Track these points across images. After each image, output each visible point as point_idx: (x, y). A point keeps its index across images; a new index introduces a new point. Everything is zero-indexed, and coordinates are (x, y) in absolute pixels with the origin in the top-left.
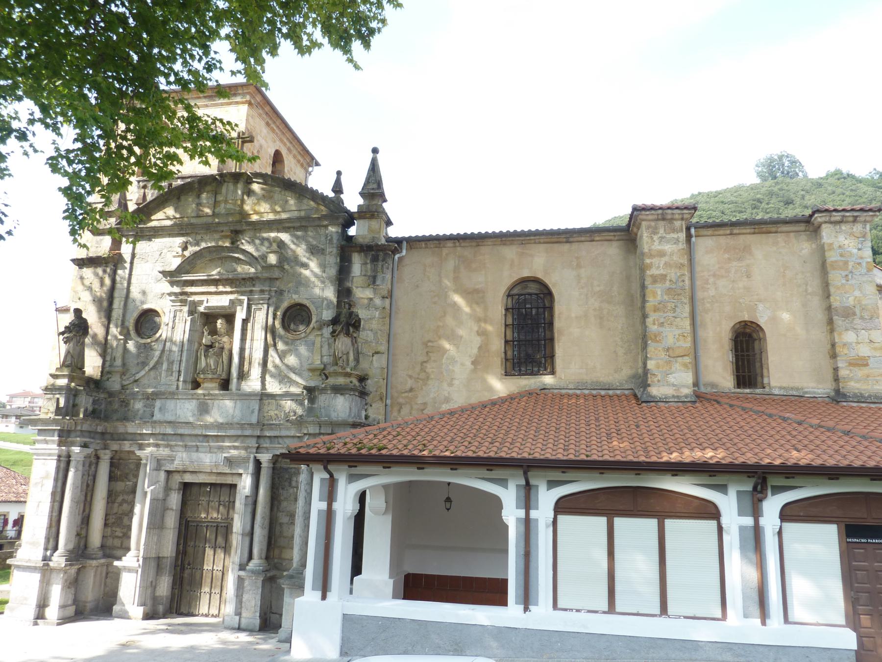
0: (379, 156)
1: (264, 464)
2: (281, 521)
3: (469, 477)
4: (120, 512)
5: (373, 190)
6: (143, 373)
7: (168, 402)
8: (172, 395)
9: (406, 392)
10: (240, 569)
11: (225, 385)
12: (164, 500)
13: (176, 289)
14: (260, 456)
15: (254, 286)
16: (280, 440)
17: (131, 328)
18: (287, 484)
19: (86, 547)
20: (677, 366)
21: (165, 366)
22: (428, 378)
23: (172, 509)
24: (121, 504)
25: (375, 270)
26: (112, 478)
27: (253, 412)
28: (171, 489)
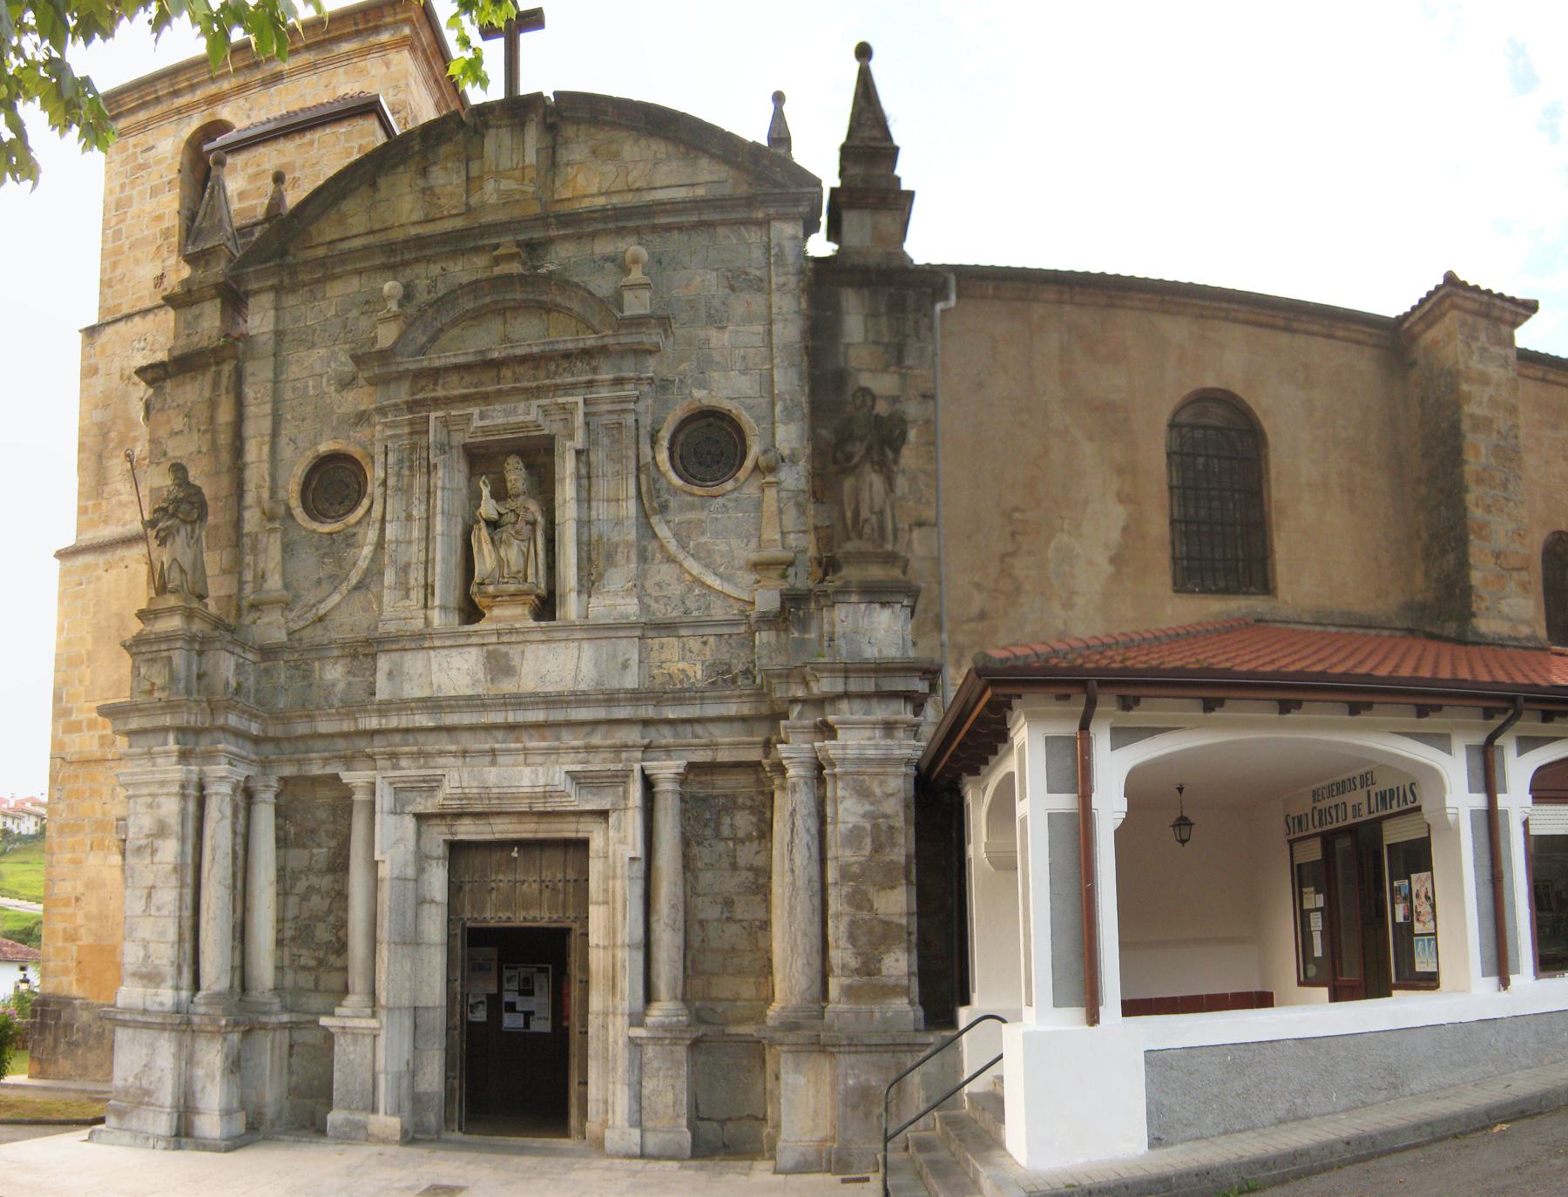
0: (874, 65)
1: (666, 787)
2: (701, 916)
3: (1375, 728)
4: (306, 914)
5: (869, 143)
6: (336, 598)
7: (408, 656)
8: (420, 640)
9: (971, 620)
10: (631, 1025)
11: (546, 607)
13: (402, 393)
14: (653, 767)
16: (699, 729)
17: (295, 503)
18: (708, 832)
19: (244, 988)
20: (1512, 586)
21: (389, 577)
22: (1018, 590)
24: (305, 897)
26: (282, 842)
27: (625, 666)
28: (428, 857)
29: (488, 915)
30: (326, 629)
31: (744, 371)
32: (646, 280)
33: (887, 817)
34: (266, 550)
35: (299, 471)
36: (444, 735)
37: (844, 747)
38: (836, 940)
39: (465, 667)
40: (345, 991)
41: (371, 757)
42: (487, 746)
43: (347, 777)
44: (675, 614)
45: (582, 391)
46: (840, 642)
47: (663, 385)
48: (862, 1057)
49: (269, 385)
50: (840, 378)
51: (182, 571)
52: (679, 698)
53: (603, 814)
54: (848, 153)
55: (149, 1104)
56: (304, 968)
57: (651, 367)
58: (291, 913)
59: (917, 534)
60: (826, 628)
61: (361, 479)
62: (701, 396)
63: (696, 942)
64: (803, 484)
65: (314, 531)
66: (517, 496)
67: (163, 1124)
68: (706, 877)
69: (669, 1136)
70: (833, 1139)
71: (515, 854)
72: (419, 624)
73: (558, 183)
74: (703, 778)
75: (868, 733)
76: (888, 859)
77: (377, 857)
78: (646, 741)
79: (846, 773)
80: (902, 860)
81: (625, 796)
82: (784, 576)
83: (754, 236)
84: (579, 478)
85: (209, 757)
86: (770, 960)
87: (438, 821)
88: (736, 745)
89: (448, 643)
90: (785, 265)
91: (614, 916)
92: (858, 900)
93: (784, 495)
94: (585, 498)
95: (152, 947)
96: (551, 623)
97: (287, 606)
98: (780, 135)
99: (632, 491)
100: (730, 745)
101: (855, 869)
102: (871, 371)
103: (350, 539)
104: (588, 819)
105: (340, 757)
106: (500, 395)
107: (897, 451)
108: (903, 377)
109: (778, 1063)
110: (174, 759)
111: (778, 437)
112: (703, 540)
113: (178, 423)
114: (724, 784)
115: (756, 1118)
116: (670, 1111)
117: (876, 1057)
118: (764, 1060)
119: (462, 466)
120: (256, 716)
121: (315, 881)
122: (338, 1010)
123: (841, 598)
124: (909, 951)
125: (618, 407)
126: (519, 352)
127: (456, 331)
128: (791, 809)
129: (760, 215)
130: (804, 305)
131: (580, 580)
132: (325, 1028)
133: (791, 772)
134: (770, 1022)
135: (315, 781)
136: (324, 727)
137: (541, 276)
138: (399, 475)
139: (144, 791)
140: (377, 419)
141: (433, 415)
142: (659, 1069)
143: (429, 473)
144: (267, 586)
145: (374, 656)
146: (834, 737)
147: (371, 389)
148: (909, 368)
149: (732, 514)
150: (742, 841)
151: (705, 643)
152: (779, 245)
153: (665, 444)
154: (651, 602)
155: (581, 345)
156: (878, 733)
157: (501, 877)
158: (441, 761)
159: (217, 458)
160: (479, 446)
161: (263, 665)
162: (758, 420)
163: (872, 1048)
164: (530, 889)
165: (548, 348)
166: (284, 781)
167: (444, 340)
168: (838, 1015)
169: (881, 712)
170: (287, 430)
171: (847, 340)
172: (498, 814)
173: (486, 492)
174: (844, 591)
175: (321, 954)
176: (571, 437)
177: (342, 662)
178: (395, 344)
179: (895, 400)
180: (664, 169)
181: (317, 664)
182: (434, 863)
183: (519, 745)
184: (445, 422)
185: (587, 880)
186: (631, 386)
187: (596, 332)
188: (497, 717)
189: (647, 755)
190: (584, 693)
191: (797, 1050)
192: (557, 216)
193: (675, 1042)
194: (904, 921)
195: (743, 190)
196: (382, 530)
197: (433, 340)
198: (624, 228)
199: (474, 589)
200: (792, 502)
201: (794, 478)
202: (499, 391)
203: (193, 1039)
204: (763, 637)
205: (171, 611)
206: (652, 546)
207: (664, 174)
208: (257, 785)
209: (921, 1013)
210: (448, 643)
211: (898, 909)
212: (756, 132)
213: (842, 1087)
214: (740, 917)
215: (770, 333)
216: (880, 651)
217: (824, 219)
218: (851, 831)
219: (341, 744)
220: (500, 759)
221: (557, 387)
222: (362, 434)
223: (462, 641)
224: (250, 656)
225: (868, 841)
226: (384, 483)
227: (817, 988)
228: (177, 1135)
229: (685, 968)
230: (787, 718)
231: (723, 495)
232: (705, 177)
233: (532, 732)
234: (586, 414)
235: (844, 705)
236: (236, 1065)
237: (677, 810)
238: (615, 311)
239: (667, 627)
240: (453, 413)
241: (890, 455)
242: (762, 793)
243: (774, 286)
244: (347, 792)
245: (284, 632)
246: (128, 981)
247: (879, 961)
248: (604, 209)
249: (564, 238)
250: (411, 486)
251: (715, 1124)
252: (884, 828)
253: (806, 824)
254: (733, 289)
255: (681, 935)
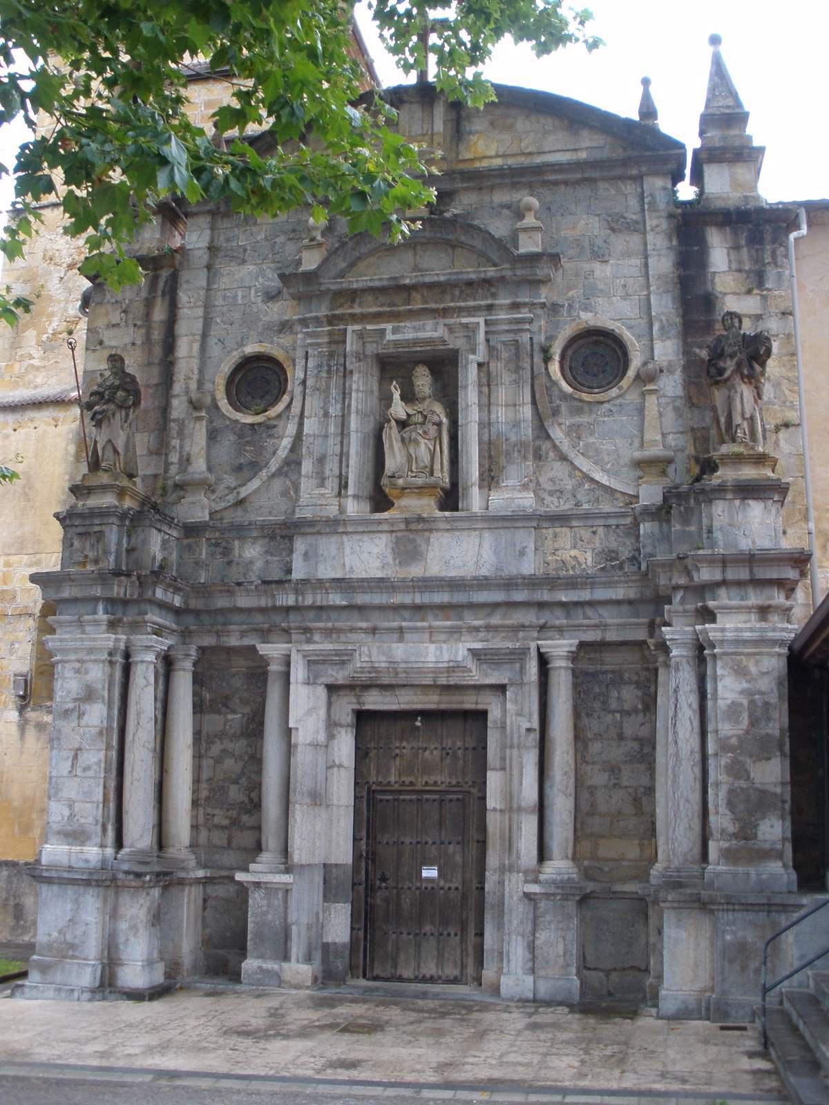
0: (723, 49)
2: (590, 783)
5: (724, 116)
6: (255, 484)
8: (335, 526)
11: (450, 499)
12: (327, 746)
15: (494, 296)
18: (597, 705)
21: (307, 467)
23: (340, 766)
24: (218, 761)
25: (758, 260)
26: (199, 708)
27: (522, 553)
29: (392, 779)
30: (246, 510)
31: (626, 297)
32: (539, 224)
33: (762, 693)
34: (192, 435)
35: (226, 368)
36: (356, 614)
37: (723, 630)
38: (717, 806)
39: (375, 550)
40: (258, 848)
41: (287, 631)
42: (395, 624)
43: (264, 649)
44: (567, 506)
45: (484, 313)
46: (718, 535)
47: (554, 309)
48: (739, 915)
49: (202, 293)
50: (709, 302)
51: (116, 451)
52: (572, 583)
53: (502, 688)
54: (708, 121)
55: (73, 957)
56: (217, 827)
57: (544, 295)
58: (205, 775)
59: (782, 434)
60: (705, 521)
61: (282, 378)
62: (588, 319)
63: (585, 807)
64: (679, 391)
65: (237, 421)
66: (424, 399)
67: (87, 977)
68: (595, 747)
69: (561, 983)
70: (712, 989)
71: (418, 724)
72: (333, 511)
73: (461, 148)
74: (592, 656)
75: (743, 617)
76: (763, 732)
77: (291, 725)
78: (542, 621)
79: (724, 654)
80: (777, 733)
81: (522, 670)
82: (664, 473)
83: (630, 188)
84: (480, 386)
85: (135, 627)
86: (654, 823)
87: (347, 692)
88: (623, 626)
89: (361, 529)
90: (657, 211)
91: (511, 780)
92: (737, 770)
93: (663, 400)
94: (487, 405)
95: (77, 806)
96: (456, 514)
97: (210, 488)
98: (648, 111)
99: (528, 398)
100: (617, 626)
101: (734, 741)
102: (735, 293)
103: (268, 427)
104: (488, 692)
105: (256, 630)
106: (412, 314)
107: (763, 365)
108: (764, 298)
109: (661, 918)
110: (104, 628)
111: (656, 352)
112: (591, 440)
113: (116, 317)
114: (612, 660)
115: (639, 970)
116: (561, 960)
117: (751, 916)
118: (647, 916)
119: (376, 372)
120: (180, 589)
121: (230, 746)
122: (252, 867)
123: (717, 495)
124: (783, 818)
125: (514, 327)
126: (427, 279)
127: (373, 260)
128: (678, 682)
129: (634, 172)
130: (675, 242)
131: (481, 475)
132: (240, 883)
133: (675, 652)
134: (653, 881)
135: (230, 651)
136: (243, 601)
137: (446, 220)
138: (317, 376)
139: (73, 657)
140: (298, 328)
141: (350, 328)
142: (550, 923)
143: (345, 376)
144: (190, 469)
145: (291, 539)
146: (714, 620)
147: (295, 303)
148: (768, 290)
149: (617, 417)
150: (628, 713)
151: (594, 533)
152: (651, 195)
153: (557, 358)
154: (546, 496)
155: (483, 276)
156: (753, 617)
157: (404, 744)
158: (354, 637)
159: (150, 352)
160: (389, 356)
161: (185, 542)
162: (638, 337)
163: (749, 907)
164: (432, 755)
165: (453, 277)
166: (202, 650)
167: (361, 266)
168: (718, 875)
169: (755, 598)
170: (215, 332)
171: (713, 270)
172: (404, 686)
173: (397, 395)
174: (721, 490)
175: (234, 813)
176: (473, 351)
177: (261, 542)
178: (319, 267)
179: (759, 317)
180: (552, 138)
181: (236, 543)
182: (343, 731)
183: (425, 624)
184: (361, 335)
185: (485, 748)
186: (526, 310)
187: (495, 265)
188: (407, 599)
189: (543, 635)
190: (486, 578)
191: (681, 906)
192: (462, 173)
193: (565, 897)
194: (778, 790)
195: (619, 153)
196: (301, 424)
197: (352, 265)
198: (518, 183)
199: (384, 481)
200: (671, 406)
201: (672, 385)
202: (410, 311)
203: (117, 893)
204: (645, 528)
205: (104, 488)
206: (546, 446)
207: (551, 142)
208: (178, 654)
209: (794, 876)
210: (361, 529)
211: (774, 780)
212: (629, 110)
213: (719, 943)
214: (625, 783)
215: (646, 265)
216: (754, 542)
217: (688, 172)
218: (729, 707)
219: (259, 618)
220: (407, 636)
221: (461, 309)
222: (286, 340)
223: (374, 528)
224: (175, 533)
225: (745, 715)
226: (304, 382)
227: (697, 851)
228: (102, 985)
229: (575, 830)
230: (670, 602)
231: (608, 402)
232: (587, 144)
233: (436, 612)
234: (486, 333)
235: (722, 592)
236: (157, 918)
237: (570, 685)
238: (512, 249)
239: (560, 519)
240: (369, 327)
241: (758, 368)
242: (647, 669)
243: (648, 228)
244: (264, 662)
245: (207, 512)
246: (53, 839)
247: (756, 826)
248: (501, 169)
249: (466, 189)
250: (328, 387)
251: (601, 974)
252: (759, 704)
253: (688, 700)
254: (613, 230)
255: (572, 799)
